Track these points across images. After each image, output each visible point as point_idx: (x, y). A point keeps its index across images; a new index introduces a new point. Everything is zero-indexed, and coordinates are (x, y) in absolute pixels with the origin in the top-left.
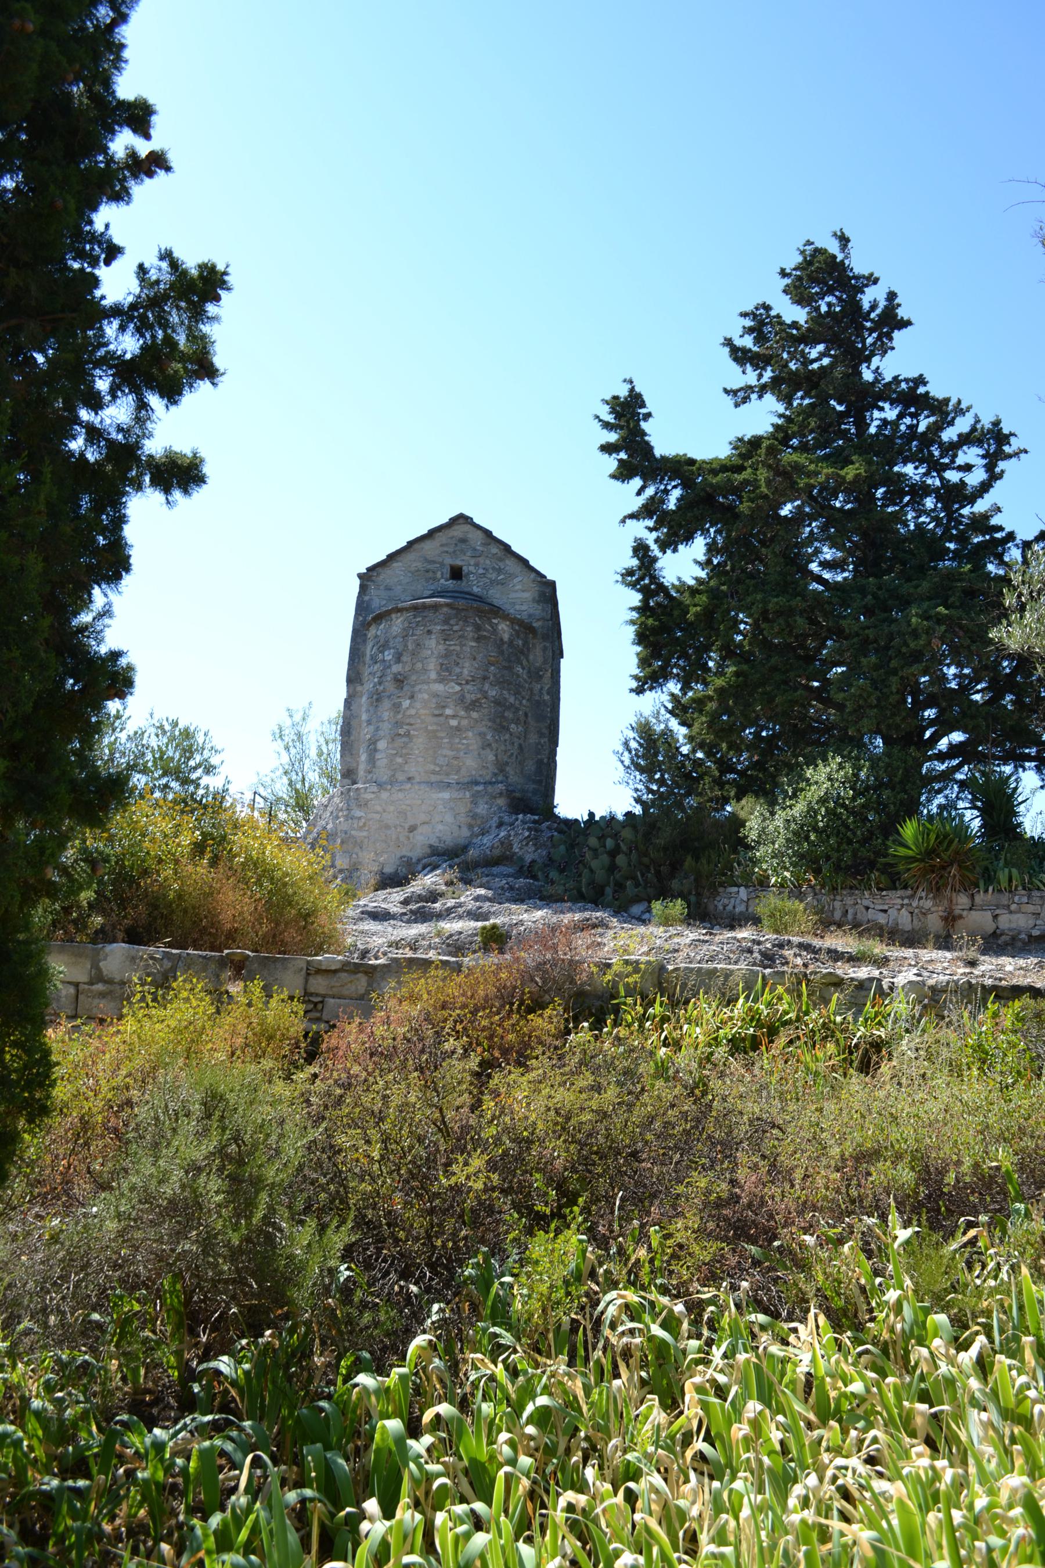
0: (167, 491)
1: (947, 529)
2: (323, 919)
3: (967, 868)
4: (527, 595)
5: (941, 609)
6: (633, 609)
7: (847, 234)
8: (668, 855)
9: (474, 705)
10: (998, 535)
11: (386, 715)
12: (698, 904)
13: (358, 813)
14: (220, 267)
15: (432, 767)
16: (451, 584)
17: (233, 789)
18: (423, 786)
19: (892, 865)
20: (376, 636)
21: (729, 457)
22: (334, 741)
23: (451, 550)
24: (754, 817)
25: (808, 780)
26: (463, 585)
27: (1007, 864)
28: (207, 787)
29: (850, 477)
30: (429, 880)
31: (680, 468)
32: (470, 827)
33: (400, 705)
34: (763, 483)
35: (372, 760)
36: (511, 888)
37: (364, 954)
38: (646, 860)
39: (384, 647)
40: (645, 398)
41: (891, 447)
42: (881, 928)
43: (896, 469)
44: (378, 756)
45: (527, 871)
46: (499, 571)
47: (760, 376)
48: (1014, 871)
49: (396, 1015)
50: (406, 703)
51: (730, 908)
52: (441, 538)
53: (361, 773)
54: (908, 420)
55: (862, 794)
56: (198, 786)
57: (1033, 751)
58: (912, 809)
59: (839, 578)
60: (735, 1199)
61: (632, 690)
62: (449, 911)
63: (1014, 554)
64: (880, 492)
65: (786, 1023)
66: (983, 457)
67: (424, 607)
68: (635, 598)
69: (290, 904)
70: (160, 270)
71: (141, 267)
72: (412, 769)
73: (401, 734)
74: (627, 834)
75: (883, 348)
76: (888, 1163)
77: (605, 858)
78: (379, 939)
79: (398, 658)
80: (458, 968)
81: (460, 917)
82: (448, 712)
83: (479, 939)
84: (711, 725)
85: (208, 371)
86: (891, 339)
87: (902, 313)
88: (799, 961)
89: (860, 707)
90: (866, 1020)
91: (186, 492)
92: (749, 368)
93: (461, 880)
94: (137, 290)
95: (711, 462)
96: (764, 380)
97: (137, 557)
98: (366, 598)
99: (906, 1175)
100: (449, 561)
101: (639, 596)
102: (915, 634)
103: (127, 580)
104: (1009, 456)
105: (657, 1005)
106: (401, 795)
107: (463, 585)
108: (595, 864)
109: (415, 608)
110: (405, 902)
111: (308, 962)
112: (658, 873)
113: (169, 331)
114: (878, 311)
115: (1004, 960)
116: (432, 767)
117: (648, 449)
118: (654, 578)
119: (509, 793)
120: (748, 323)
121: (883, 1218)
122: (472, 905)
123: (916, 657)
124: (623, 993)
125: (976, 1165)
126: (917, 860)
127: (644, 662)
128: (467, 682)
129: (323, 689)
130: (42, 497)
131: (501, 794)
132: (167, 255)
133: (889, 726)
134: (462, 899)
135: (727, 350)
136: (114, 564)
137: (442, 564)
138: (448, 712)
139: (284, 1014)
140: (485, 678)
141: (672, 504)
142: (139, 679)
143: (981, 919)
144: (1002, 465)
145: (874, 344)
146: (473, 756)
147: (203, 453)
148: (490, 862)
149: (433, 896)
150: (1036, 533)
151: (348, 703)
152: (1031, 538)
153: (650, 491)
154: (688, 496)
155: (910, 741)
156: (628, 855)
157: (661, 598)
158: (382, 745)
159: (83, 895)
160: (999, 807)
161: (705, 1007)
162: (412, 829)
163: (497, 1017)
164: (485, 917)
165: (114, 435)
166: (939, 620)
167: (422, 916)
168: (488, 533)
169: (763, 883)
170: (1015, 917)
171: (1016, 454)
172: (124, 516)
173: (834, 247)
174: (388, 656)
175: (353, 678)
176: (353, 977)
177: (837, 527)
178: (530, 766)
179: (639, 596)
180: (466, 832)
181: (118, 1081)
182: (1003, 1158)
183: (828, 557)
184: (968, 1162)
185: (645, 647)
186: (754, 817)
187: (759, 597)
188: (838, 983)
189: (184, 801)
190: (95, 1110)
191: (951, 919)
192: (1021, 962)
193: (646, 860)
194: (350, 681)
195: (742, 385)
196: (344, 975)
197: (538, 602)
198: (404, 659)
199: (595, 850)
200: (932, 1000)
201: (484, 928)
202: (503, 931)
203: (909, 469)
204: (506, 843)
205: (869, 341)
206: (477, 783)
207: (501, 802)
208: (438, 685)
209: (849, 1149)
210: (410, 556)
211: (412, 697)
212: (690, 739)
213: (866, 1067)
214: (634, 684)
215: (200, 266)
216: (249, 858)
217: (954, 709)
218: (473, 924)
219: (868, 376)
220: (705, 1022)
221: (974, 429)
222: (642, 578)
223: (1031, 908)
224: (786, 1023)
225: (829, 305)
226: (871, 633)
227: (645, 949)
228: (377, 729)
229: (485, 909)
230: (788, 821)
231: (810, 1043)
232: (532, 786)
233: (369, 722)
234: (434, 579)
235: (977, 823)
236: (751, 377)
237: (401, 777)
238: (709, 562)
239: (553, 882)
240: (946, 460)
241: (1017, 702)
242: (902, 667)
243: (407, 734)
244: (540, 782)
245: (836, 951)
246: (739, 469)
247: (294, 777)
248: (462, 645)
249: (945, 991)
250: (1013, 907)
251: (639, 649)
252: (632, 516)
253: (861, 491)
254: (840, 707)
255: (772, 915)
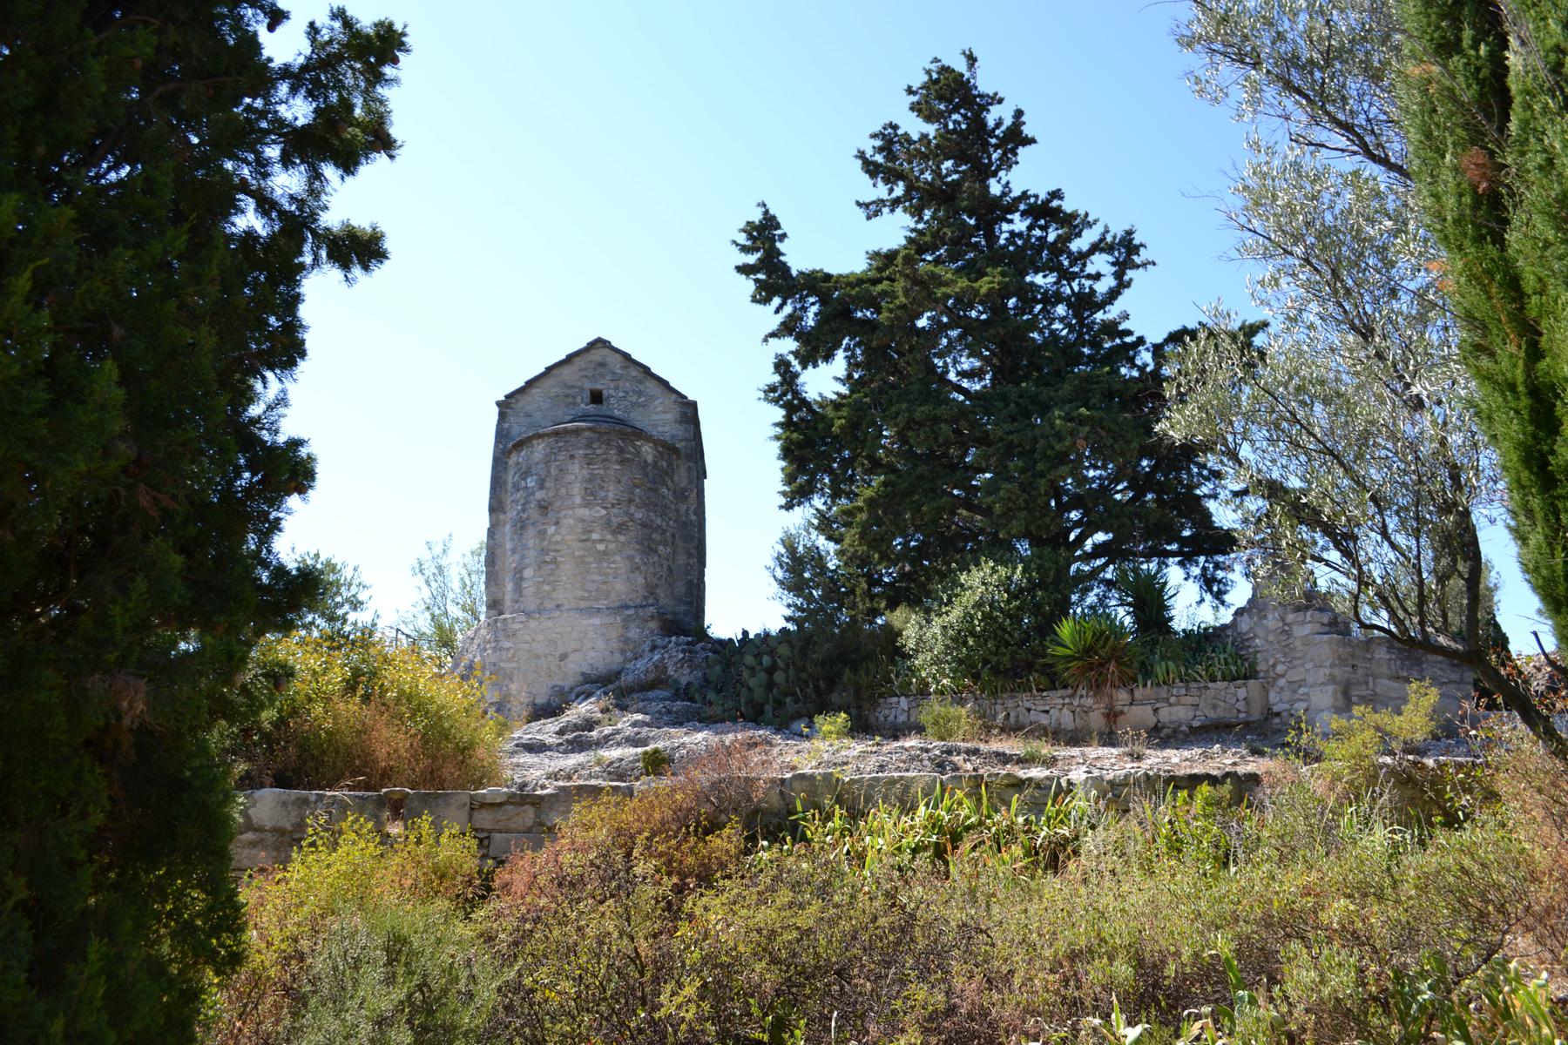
0: (346, 266)
1: (1080, 335)
2: (481, 752)
3: (1124, 664)
4: (668, 416)
5: (1083, 410)
6: (776, 425)
7: (975, 54)
8: (828, 665)
9: (620, 529)
10: (1128, 340)
11: (531, 543)
12: (859, 717)
13: (507, 644)
14: (398, 27)
15: (581, 593)
16: (591, 408)
17: (380, 624)
18: (572, 613)
19: (1051, 666)
20: (518, 463)
21: (865, 272)
22: (477, 572)
23: (589, 374)
24: (909, 625)
25: (962, 585)
26: (603, 409)
27: (1163, 657)
28: (355, 624)
29: (983, 291)
30: (583, 709)
31: (817, 283)
32: (623, 652)
33: (545, 531)
34: (900, 293)
35: (518, 589)
36: (669, 712)
37: (523, 786)
38: (804, 675)
39: (526, 474)
40: (780, 219)
41: (1026, 256)
42: (1045, 729)
43: (1028, 279)
44: (524, 585)
45: (684, 693)
46: (640, 393)
47: (891, 191)
48: (1170, 664)
49: (580, 839)
50: (551, 530)
51: (891, 718)
52: (580, 362)
53: (508, 603)
54: (1037, 232)
55: (1016, 597)
56: (345, 621)
57: (1174, 547)
58: (1063, 608)
59: (978, 387)
60: (951, 1010)
61: (781, 507)
62: (607, 738)
63: (1145, 357)
64: (1012, 302)
65: (968, 828)
66: (1113, 264)
67: (566, 431)
68: (779, 414)
69: (447, 738)
70: (332, 29)
71: (312, 25)
72: (560, 596)
73: (547, 560)
74: (784, 650)
75: (1007, 162)
76: (1105, 960)
77: (762, 676)
78: (537, 772)
79: (541, 485)
80: (630, 792)
81: (619, 744)
82: (595, 536)
83: (641, 764)
84: (862, 536)
85: (383, 142)
86: (1016, 154)
87: (1027, 130)
88: (969, 766)
89: (1010, 509)
90: (1049, 819)
91: (366, 268)
92: (880, 184)
93: (617, 706)
94: (308, 51)
95: (847, 276)
96: (894, 195)
97: (311, 340)
98: (506, 426)
99: (1123, 970)
100: (588, 385)
101: (783, 412)
102: (1059, 437)
103: (302, 365)
104: (1138, 266)
105: (836, 819)
106: (550, 624)
107: (603, 409)
108: (752, 682)
109: (556, 433)
110: (561, 732)
111: (472, 797)
112: (817, 688)
113: (345, 93)
114: (1003, 128)
115: (1169, 752)
116: (581, 593)
117: (785, 269)
118: (796, 394)
119: (661, 616)
120: (878, 143)
121: (1106, 1017)
122: (630, 731)
123: (1062, 458)
124: (800, 808)
125: (1196, 955)
126: (1075, 659)
127: (790, 479)
128: (613, 506)
129: (466, 521)
130: (215, 262)
131: (652, 617)
132: (339, 14)
133: (1039, 528)
134: (619, 726)
135: (859, 162)
136: (287, 350)
137: (582, 389)
138: (595, 536)
139: (455, 849)
140: (630, 501)
141: (810, 321)
142: (320, 469)
143: (1143, 713)
144: (1130, 274)
145: (1000, 159)
146: (621, 577)
147: (383, 227)
148: (645, 687)
149: (589, 725)
150: (1165, 335)
151: (491, 532)
152: (1159, 340)
153: (788, 309)
154: (823, 311)
155: (1054, 542)
156: (786, 671)
157: (803, 413)
158: (528, 573)
159: (265, 715)
160: (1150, 603)
161: (882, 817)
162: (563, 657)
163: (673, 842)
164: (643, 742)
165: (287, 207)
166: (1082, 421)
167: (579, 746)
168: (627, 356)
169: (923, 691)
170: (1175, 709)
171: (1144, 265)
172: (299, 294)
173: (960, 66)
174: (531, 482)
175: (496, 507)
176: (520, 809)
177: (974, 337)
178: (680, 588)
179: (783, 412)
180: (618, 658)
181: (291, 929)
182: (1223, 945)
183: (966, 367)
184: (1186, 954)
185: (791, 462)
186: (909, 625)
187: (904, 406)
188: (1019, 785)
189: (332, 639)
190: (267, 964)
191: (1112, 715)
192: (1186, 753)
193: (804, 675)
194: (492, 510)
195: (874, 198)
196: (510, 808)
197: (680, 423)
198: (548, 485)
199: (752, 669)
200: (1115, 795)
201: (646, 753)
202: (665, 755)
203: (1039, 279)
204: (661, 667)
205: (995, 156)
206: (628, 607)
207: (653, 625)
208: (582, 512)
209: (1062, 947)
210: (548, 382)
211: (557, 523)
212: (839, 553)
213: (1054, 865)
214: (783, 501)
215: (376, 25)
216: (401, 692)
217: (1097, 508)
218: (633, 750)
219: (995, 188)
220: (886, 833)
221: (1103, 239)
222: (785, 394)
223: (1189, 700)
224: (968, 828)
225: (955, 122)
226: (1014, 438)
227: (814, 763)
228: (523, 557)
229: (643, 735)
230: (944, 628)
231: (995, 847)
232: (682, 608)
233: (514, 551)
234: (574, 404)
235: (1128, 620)
236: (881, 191)
237: (549, 604)
238: (850, 376)
239: (710, 703)
240: (1076, 269)
241: (1158, 500)
242: (1049, 470)
243: (554, 561)
244: (690, 603)
245: (1004, 754)
246: (878, 281)
247: (437, 612)
248: (606, 469)
249: (1126, 785)
250: (1173, 700)
251: (783, 464)
252: (773, 335)
253: (995, 302)
254: (987, 512)
255: (936, 723)
